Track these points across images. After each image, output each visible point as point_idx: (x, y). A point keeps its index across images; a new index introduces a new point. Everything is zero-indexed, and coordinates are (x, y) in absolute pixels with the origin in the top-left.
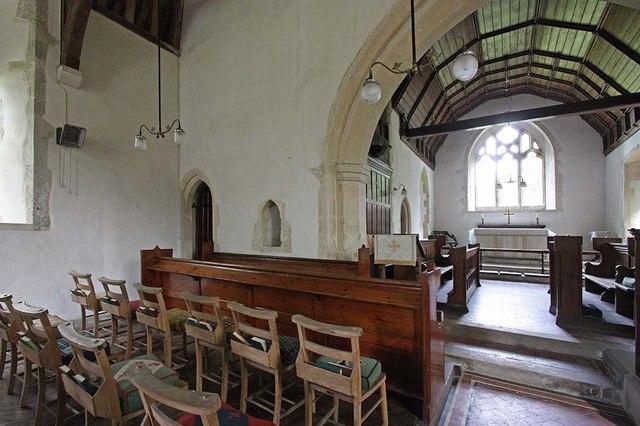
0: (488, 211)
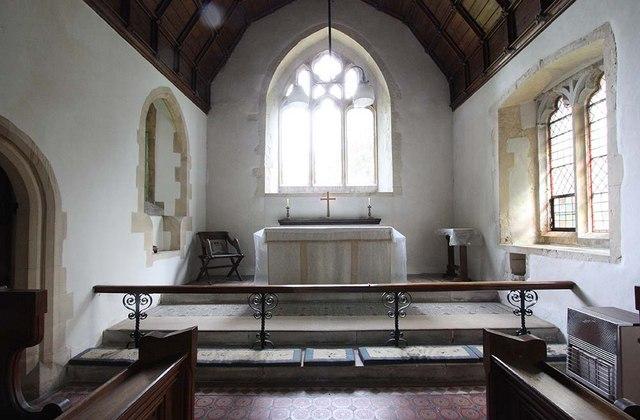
0: (298, 194)
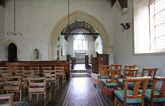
0: (77, 51)
